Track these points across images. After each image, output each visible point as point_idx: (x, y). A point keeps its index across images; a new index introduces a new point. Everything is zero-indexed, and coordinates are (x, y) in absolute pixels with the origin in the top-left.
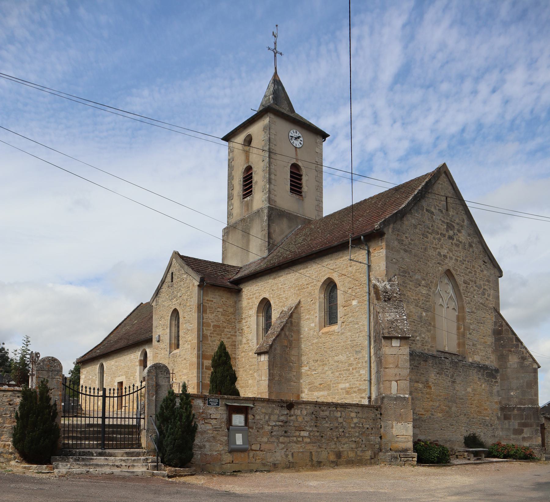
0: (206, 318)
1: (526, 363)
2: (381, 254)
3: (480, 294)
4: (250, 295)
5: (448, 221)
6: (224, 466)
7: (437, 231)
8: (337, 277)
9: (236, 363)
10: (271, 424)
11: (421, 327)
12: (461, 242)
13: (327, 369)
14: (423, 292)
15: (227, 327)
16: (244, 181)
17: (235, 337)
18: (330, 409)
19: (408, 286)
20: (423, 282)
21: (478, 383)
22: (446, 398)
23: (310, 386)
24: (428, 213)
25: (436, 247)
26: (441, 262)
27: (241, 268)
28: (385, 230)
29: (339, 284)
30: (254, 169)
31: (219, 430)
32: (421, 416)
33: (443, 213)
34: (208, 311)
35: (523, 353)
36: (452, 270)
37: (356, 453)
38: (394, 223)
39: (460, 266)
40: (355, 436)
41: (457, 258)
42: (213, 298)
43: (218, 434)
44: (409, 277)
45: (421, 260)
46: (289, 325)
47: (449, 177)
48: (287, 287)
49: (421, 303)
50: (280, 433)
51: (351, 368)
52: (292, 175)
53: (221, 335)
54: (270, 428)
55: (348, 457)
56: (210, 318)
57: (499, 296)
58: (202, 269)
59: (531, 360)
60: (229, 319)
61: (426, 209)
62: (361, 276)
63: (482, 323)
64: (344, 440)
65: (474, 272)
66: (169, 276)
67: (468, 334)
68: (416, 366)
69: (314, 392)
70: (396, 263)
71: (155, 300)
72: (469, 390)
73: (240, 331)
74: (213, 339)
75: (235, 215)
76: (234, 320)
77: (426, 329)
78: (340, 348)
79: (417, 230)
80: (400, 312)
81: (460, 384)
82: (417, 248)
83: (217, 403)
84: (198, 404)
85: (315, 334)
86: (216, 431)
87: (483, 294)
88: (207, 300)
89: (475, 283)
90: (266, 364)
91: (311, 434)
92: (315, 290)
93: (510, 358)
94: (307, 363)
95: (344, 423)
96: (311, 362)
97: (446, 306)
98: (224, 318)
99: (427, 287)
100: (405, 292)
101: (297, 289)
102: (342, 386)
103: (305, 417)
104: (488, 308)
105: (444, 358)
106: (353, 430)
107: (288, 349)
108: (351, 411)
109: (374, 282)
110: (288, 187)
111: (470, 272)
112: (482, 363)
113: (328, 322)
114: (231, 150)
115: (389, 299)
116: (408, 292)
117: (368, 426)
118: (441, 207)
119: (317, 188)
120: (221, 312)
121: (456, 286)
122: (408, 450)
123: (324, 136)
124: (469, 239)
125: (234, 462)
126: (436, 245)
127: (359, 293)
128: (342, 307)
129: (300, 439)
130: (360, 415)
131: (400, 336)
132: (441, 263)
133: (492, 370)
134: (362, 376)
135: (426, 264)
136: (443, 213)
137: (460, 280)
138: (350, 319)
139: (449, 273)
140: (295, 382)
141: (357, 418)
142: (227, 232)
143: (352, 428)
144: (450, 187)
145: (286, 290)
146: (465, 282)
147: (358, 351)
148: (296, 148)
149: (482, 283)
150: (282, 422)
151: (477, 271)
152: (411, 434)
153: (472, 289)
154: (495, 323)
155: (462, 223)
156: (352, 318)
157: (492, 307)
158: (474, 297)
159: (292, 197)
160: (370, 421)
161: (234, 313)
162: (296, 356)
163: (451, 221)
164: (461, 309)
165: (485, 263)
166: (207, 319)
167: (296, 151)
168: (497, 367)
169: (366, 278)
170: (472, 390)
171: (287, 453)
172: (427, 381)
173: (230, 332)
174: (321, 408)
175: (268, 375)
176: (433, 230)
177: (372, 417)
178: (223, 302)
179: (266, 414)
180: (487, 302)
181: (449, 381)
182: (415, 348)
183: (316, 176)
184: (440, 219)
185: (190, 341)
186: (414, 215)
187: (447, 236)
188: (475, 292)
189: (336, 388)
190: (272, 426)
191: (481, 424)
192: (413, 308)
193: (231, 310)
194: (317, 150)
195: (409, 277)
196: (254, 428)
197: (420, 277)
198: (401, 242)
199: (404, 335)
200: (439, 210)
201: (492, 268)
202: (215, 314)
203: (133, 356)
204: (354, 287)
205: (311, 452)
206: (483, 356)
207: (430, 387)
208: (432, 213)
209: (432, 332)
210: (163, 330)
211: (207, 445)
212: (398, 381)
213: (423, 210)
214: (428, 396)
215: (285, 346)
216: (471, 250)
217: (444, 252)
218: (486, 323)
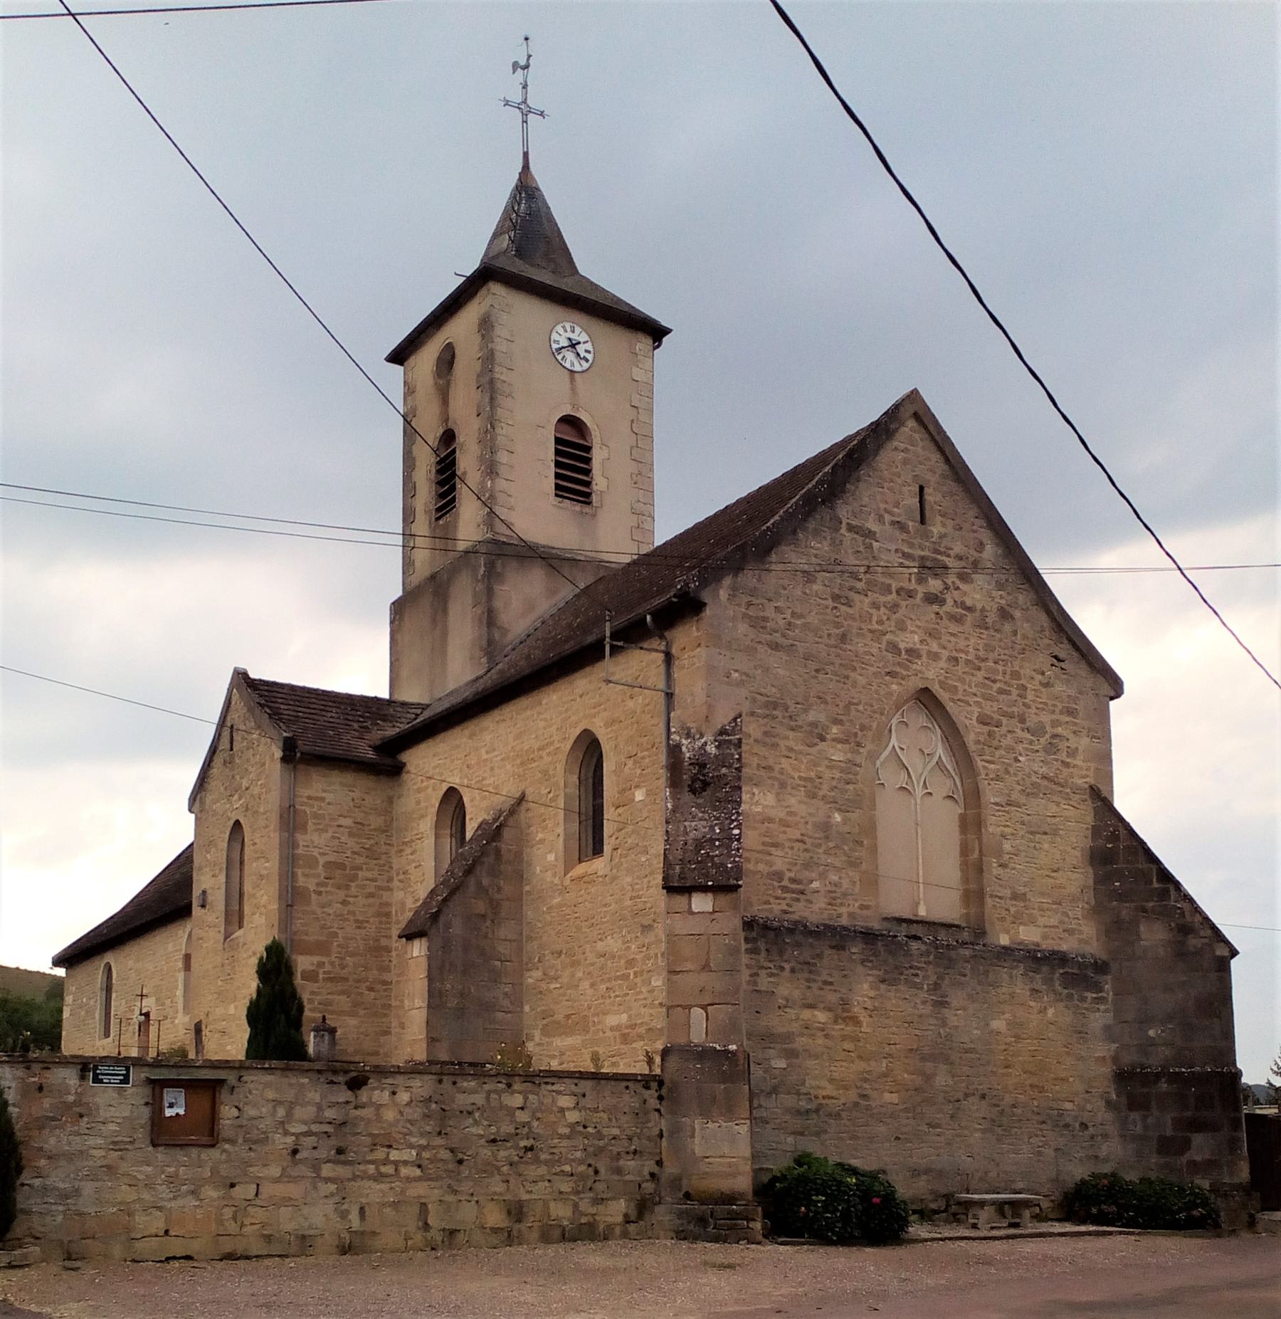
0: (305, 844)
1: (1193, 942)
2: (695, 660)
3: (1037, 751)
4: (422, 781)
5: (926, 553)
6: (138, 1245)
7: (882, 583)
8: (603, 729)
9: (390, 961)
10: (293, 1130)
11: (825, 852)
12: (969, 609)
13: (580, 974)
14: (833, 758)
15: (364, 867)
16: (439, 472)
17: (389, 893)
18: (486, 1087)
19: (782, 743)
20: (835, 730)
21: (1032, 1004)
22: (911, 1050)
23: (545, 1022)
24: (855, 536)
25: (880, 628)
26: (898, 669)
27: (428, 706)
28: (706, 596)
29: (608, 747)
30: (461, 438)
31: (127, 1149)
32: (824, 1102)
33: (908, 532)
34: (310, 826)
35: (1183, 914)
36: (936, 688)
37: (576, 1206)
38: (738, 570)
39: (965, 676)
40: (573, 1160)
41: (955, 654)
42: (324, 791)
43: (122, 1158)
44: (784, 717)
45: (829, 668)
46: (489, 860)
47: (931, 428)
48: (499, 758)
49: (825, 787)
50: (322, 1154)
51: (632, 972)
52: (559, 447)
53: (348, 887)
54: (290, 1139)
55: (549, 1216)
56: (315, 845)
57: (1110, 751)
58: (306, 716)
59: (1209, 932)
60: (372, 845)
61: (848, 524)
62: (652, 722)
63: (1045, 833)
64: (533, 1171)
65: (1017, 688)
66: (226, 733)
67: (995, 865)
68: (808, 963)
69: (554, 1036)
70: (740, 684)
71: (199, 796)
72: (998, 1024)
73: (402, 877)
74: (324, 898)
75: (418, 564)
76: (384, 848)
77: (844, 858)
78: (608, 918)
79: (815, 587)
80: (727, 819)
81: (964, 1009)
82: (816, 636)
83: (122, 1078)
84: (60, 1081)
85: (556, 882)
86: (116, 1150)
87: (1051, 748)
88: (309, 798)
89: (1023, 721)
90: (424, 964)
91: (426, 1155)
92: (557, 764)
93: (1142, 928)
94: (540, 961)
95: (535, 1124)
96: (547, 958)
97: (919, 792)
98: (358, 843)
99: (846, 742)
100: (771, 762)
101: (518, 761)
102: (612, 1020)
103: (408, 1110)
104: (1068, 790)
105: (906, 936)
106: (565, 1143)
107: (488, 923)
108: (559, 1093)
109: (675, 737)
110: (551, 481)
111: (1001, 691)
112: (1047, 945)
113: (591, 847)
114: (409, 388)
115: (705, 785)
116: (783, 760)
117: (616, 1132)
118: (899, 515)
119: (635, 479)
120: (346, 827)
121: (953, 733)
122: (737, 1199)
123: (657, 333)
124: (1001, 597)
125: (172, 1233)
126: (880, 622)
127: (649, 770)
128: (614, 809)
129: (389, 1169)
130: (588, 1102)
131: (710, 883)
132: (897, 673)
133: (1081, 966)
134: (655, 993)
135: (847, 677)
136: (908, 532)
137: (966, 717)
138: (630, 841)
139: (926, 699)
140: (510, 1012)
141: (580, 1111)
142: (399, 610)
143: (561, 1137)
144: (935, 457)
145: (496, 765)
146: (983, 720)
147: (646, 927)
148: (571, 371)
149: (1046, 718)
150: (330, 1123)
151: (1029, 686)
152: (748, 1153)
153: (1008, 740)
154: (1096, 831)
155: (976, 554)
156: (633, 836)
157: (1087, 786)
158: (1017, 760)
159: (559, 507)
160: (624, 1119)
161: (386, 830)
162: (510, 941)
163: (937, 552)
164: (973, 797)
165: (1059, 660)
166: (308, 846)
167: (572, 380)
168: (1105, 957)
169: (662, 726)
170: (1008, 1024)
171: (345, 1207)
172: (845, 1003)
173: (375, 880)
174: (459, 1085)
175: (426, 995)
176: (868, 582)
177: (630, 1106)
178: (353, 800)
179: (277, 1103)
180: (1066, 771)
181: (924, 1003)
182: (806, 914)
183: (632, 448)
184: (897, 551)
185: (265, 906)
186: (806, 547)
187: (920, 595)
188: (1020, 747)
189: (600, 1027)
190: (297, 1135)
191: (1044, 1122)
192: (800, 802)
193: (376, 821)
194: (638, 374)
195: (784, 717)
196: (240, 1141)
197: (822, 718)
198: (758, 623)
199: (724, 882)
200: (893, 523)
201: (1083, 673)
202: (330, 834)
203: (171, 945)
204: (639, 755)
205: (424, 1204)
206: (1053, 927)
207: (855, 1021)
208: (870, 534)
209: (864, 866)
210: (213, 876)
211: (88, 1188)
212: (709, 1007)
213: (837, 530)
214: (847, 1046)
215: (477, 915)
216: (1007, 627)
217: (910, 639)
218: (1061, 832)
